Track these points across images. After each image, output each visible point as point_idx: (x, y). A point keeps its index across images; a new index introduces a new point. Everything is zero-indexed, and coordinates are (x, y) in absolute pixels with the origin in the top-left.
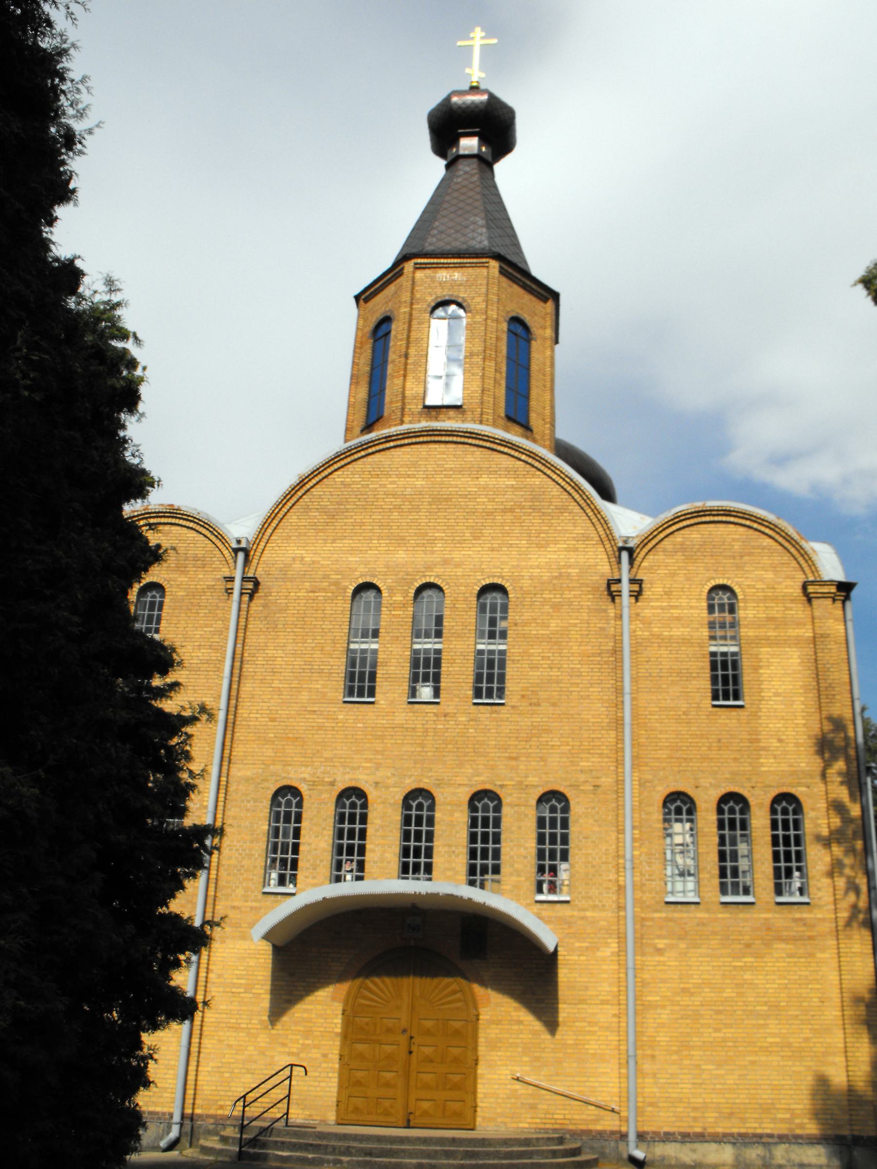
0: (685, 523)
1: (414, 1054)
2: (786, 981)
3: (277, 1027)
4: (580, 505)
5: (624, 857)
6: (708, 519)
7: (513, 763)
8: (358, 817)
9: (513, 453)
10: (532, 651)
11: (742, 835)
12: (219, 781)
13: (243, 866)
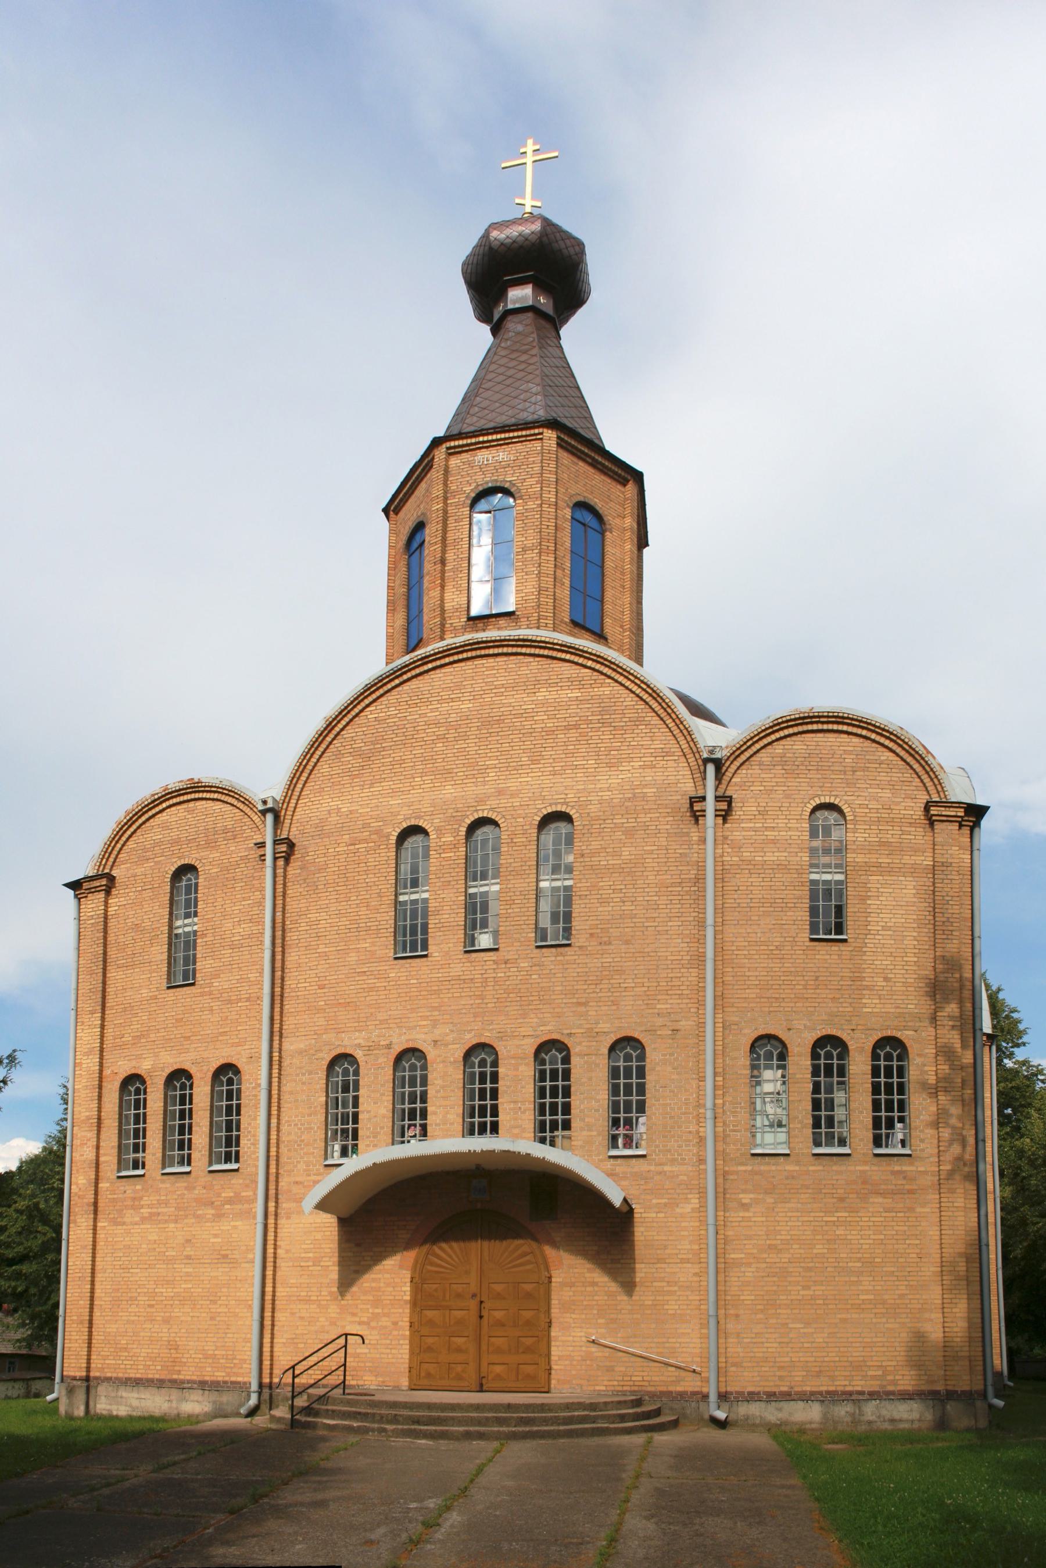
0: (786, 732)
1: (485, 1319)
2: (882, 1237)
3: (346, 1298)
4: (658, 716)
5: (704, 1106)
6: (815, 727)
7: (583, 1009)
8: (418, 1079)
9: (576, 659)
10: (601, 884)
11: (839, 1083)
12: (271, 1058)
13: (302, 1141)
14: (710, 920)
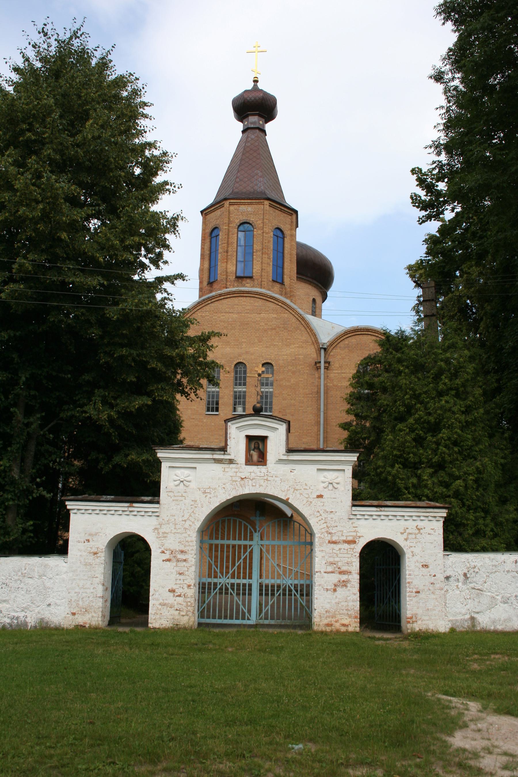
0: (349, 335)
9: (275, 302)
14: (322, 409)
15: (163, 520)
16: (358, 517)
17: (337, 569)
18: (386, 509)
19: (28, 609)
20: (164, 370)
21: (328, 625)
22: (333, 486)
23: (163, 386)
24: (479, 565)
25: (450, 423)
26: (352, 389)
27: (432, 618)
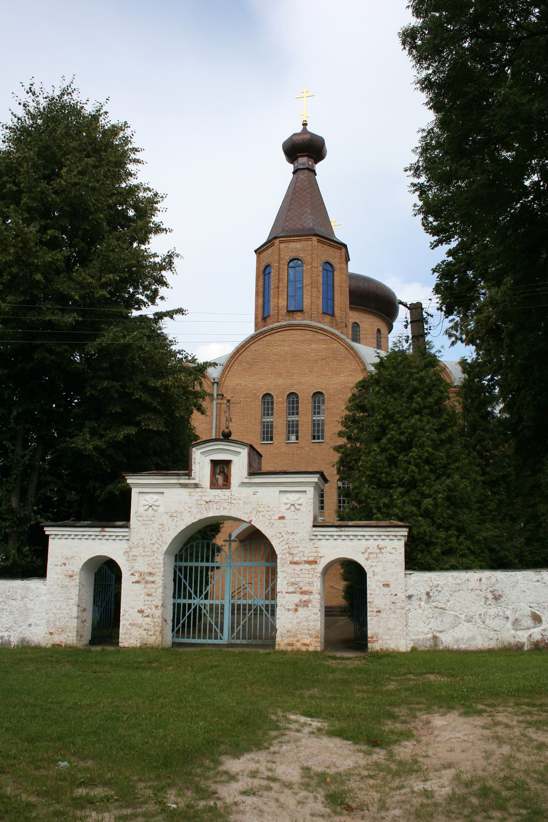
9: (325, 333)
15: (133, 543)
16: (319, 537)
17: (298, 589)
18: (346, 529)
19: (11, 629)
20: (150, 400)
21: (289, 645)
22: (295, 508)
23: (150, 416)
24: (442, 584)
25: (421, 441)
26: (347, 413)
27: (393, 637)
